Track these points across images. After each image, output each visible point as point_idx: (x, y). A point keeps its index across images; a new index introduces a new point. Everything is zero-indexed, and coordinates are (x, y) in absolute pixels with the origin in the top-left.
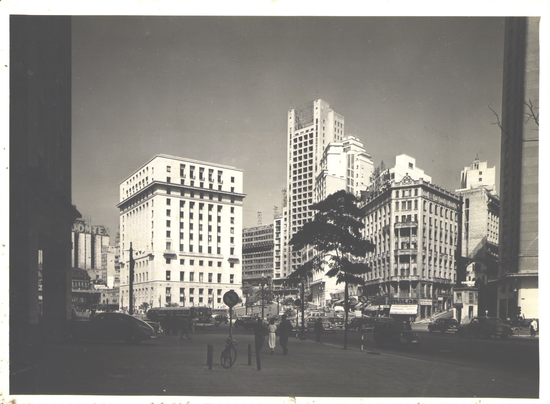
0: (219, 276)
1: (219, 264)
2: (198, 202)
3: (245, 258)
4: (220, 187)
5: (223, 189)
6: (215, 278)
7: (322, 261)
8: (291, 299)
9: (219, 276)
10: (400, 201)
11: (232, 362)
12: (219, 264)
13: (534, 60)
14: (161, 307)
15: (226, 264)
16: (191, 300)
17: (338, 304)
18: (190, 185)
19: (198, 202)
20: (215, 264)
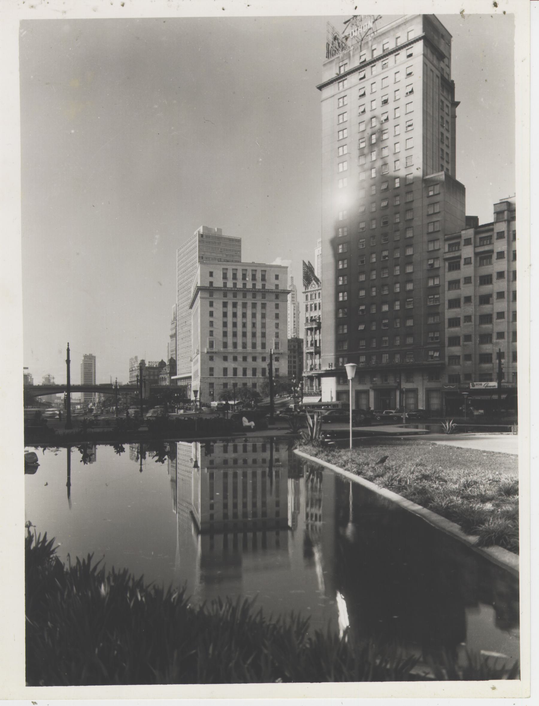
4: (264, 286)
18: (251, 287)
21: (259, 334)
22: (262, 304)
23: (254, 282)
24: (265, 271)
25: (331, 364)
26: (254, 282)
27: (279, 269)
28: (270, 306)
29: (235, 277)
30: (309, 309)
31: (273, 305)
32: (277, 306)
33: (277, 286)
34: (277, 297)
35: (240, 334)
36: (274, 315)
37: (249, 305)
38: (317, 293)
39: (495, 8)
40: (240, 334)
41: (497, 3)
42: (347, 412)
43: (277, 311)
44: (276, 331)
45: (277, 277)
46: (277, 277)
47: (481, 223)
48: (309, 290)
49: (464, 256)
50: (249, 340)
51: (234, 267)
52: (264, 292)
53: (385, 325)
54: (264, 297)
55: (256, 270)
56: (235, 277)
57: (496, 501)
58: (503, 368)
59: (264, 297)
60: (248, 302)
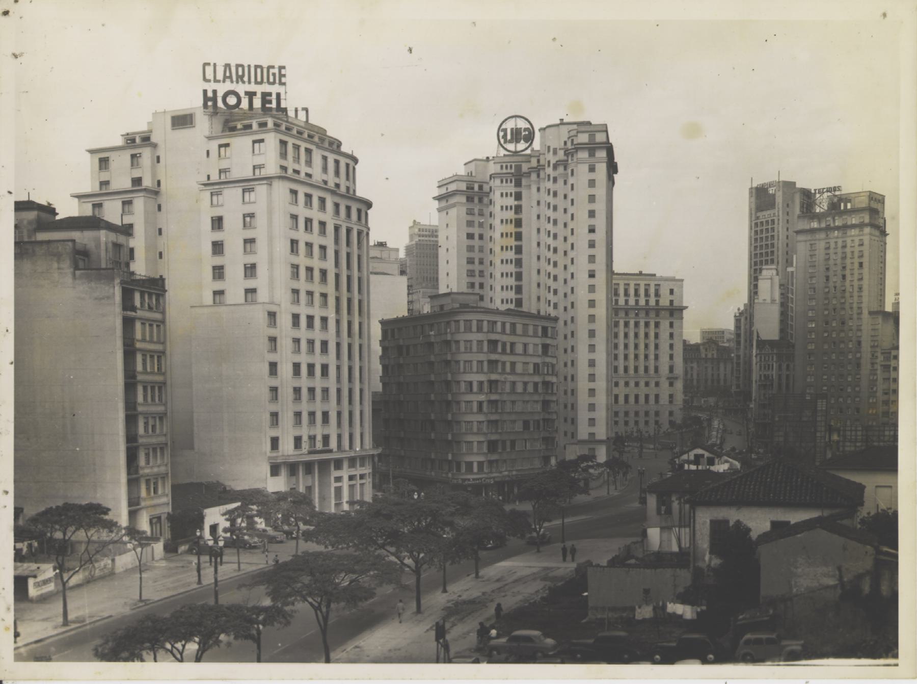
0: (657, 396)
1: (657, 384)
4: (657, 302)
9: (657, 396)
13: (734, 389)
14: (143, 598)
15: (665, 384)
16: (626, 423)
17: (716, 332)
18: (624, 304)
21: (652, 357)
23: (637, 298)
24: (659, 285)
26: (637, 298)
27: (674, 283)
29: (637, 293)
31: (667, 323)
32: (671, 325)
34: (672, 315)
35: (632, 357)
37: (642, 324)
39: (10, 14)
41: (3, 11)
45: (672, 292)
46: (672, 292)
47: (614, 175)
50: (631, 364)
51: (647, 282)
53: (825, 368)
54: (657, 315)
55: (649, 285)
56: (637, 293)
57: (338, 603)
58: (578, 454)
59: (657, 315)
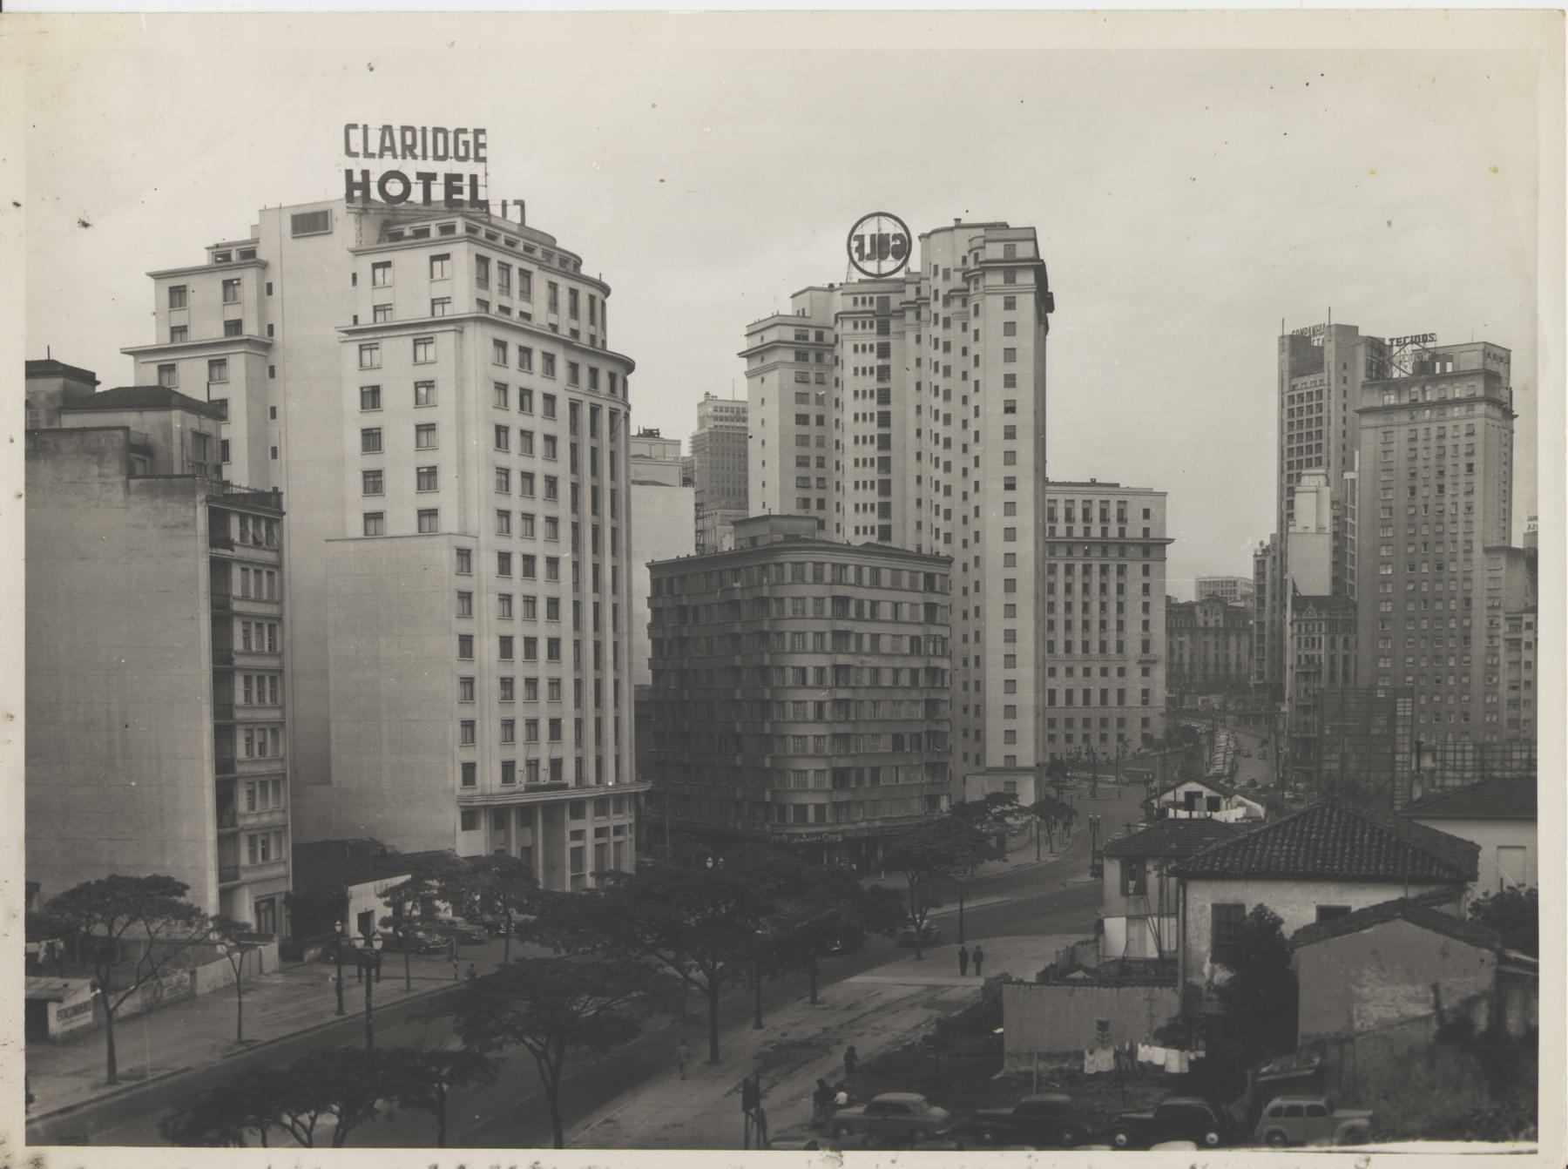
1: (1121, 672)
2: (1099, 563)
3: (597, 814)
5: (1129, 533)
6: (1113, 698)
7: (439, 889)
8: (520, 911)
10: (1303, 636)
11: (1069, 976)
12: (1121, 672)
15: (1134, 672)
19: (1099, 563)
20: (1113, 673)
22: (1119, 566)
25: (358, 178)
27: (1150, 498)
28: (1134, 569)
30: (1303, 645)
31: (1139, 568)
33: (1146, 531)
34: (1146, 553)
35: (1078, 625)
36: (1141, 586)
38: (867, 296)
40: (1078, 625)
42: (1487, 838)
43: (1146, 580)
44: (1122, 599)
45: (1146, 514)
46: (1146, 514)
48: (1304, 617)
49: (1525, 640)
51: (1068, 497)
52: (1123, 545)
54: (1122, 553)
60: (1094, 563)
